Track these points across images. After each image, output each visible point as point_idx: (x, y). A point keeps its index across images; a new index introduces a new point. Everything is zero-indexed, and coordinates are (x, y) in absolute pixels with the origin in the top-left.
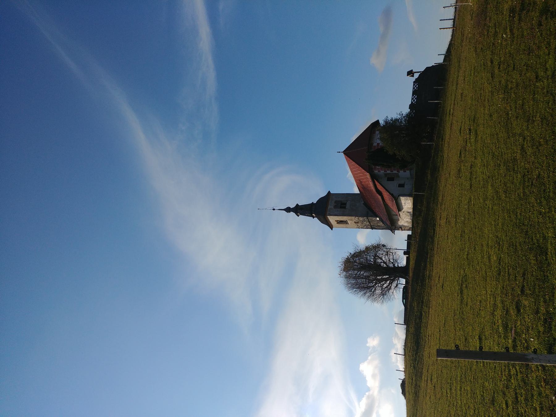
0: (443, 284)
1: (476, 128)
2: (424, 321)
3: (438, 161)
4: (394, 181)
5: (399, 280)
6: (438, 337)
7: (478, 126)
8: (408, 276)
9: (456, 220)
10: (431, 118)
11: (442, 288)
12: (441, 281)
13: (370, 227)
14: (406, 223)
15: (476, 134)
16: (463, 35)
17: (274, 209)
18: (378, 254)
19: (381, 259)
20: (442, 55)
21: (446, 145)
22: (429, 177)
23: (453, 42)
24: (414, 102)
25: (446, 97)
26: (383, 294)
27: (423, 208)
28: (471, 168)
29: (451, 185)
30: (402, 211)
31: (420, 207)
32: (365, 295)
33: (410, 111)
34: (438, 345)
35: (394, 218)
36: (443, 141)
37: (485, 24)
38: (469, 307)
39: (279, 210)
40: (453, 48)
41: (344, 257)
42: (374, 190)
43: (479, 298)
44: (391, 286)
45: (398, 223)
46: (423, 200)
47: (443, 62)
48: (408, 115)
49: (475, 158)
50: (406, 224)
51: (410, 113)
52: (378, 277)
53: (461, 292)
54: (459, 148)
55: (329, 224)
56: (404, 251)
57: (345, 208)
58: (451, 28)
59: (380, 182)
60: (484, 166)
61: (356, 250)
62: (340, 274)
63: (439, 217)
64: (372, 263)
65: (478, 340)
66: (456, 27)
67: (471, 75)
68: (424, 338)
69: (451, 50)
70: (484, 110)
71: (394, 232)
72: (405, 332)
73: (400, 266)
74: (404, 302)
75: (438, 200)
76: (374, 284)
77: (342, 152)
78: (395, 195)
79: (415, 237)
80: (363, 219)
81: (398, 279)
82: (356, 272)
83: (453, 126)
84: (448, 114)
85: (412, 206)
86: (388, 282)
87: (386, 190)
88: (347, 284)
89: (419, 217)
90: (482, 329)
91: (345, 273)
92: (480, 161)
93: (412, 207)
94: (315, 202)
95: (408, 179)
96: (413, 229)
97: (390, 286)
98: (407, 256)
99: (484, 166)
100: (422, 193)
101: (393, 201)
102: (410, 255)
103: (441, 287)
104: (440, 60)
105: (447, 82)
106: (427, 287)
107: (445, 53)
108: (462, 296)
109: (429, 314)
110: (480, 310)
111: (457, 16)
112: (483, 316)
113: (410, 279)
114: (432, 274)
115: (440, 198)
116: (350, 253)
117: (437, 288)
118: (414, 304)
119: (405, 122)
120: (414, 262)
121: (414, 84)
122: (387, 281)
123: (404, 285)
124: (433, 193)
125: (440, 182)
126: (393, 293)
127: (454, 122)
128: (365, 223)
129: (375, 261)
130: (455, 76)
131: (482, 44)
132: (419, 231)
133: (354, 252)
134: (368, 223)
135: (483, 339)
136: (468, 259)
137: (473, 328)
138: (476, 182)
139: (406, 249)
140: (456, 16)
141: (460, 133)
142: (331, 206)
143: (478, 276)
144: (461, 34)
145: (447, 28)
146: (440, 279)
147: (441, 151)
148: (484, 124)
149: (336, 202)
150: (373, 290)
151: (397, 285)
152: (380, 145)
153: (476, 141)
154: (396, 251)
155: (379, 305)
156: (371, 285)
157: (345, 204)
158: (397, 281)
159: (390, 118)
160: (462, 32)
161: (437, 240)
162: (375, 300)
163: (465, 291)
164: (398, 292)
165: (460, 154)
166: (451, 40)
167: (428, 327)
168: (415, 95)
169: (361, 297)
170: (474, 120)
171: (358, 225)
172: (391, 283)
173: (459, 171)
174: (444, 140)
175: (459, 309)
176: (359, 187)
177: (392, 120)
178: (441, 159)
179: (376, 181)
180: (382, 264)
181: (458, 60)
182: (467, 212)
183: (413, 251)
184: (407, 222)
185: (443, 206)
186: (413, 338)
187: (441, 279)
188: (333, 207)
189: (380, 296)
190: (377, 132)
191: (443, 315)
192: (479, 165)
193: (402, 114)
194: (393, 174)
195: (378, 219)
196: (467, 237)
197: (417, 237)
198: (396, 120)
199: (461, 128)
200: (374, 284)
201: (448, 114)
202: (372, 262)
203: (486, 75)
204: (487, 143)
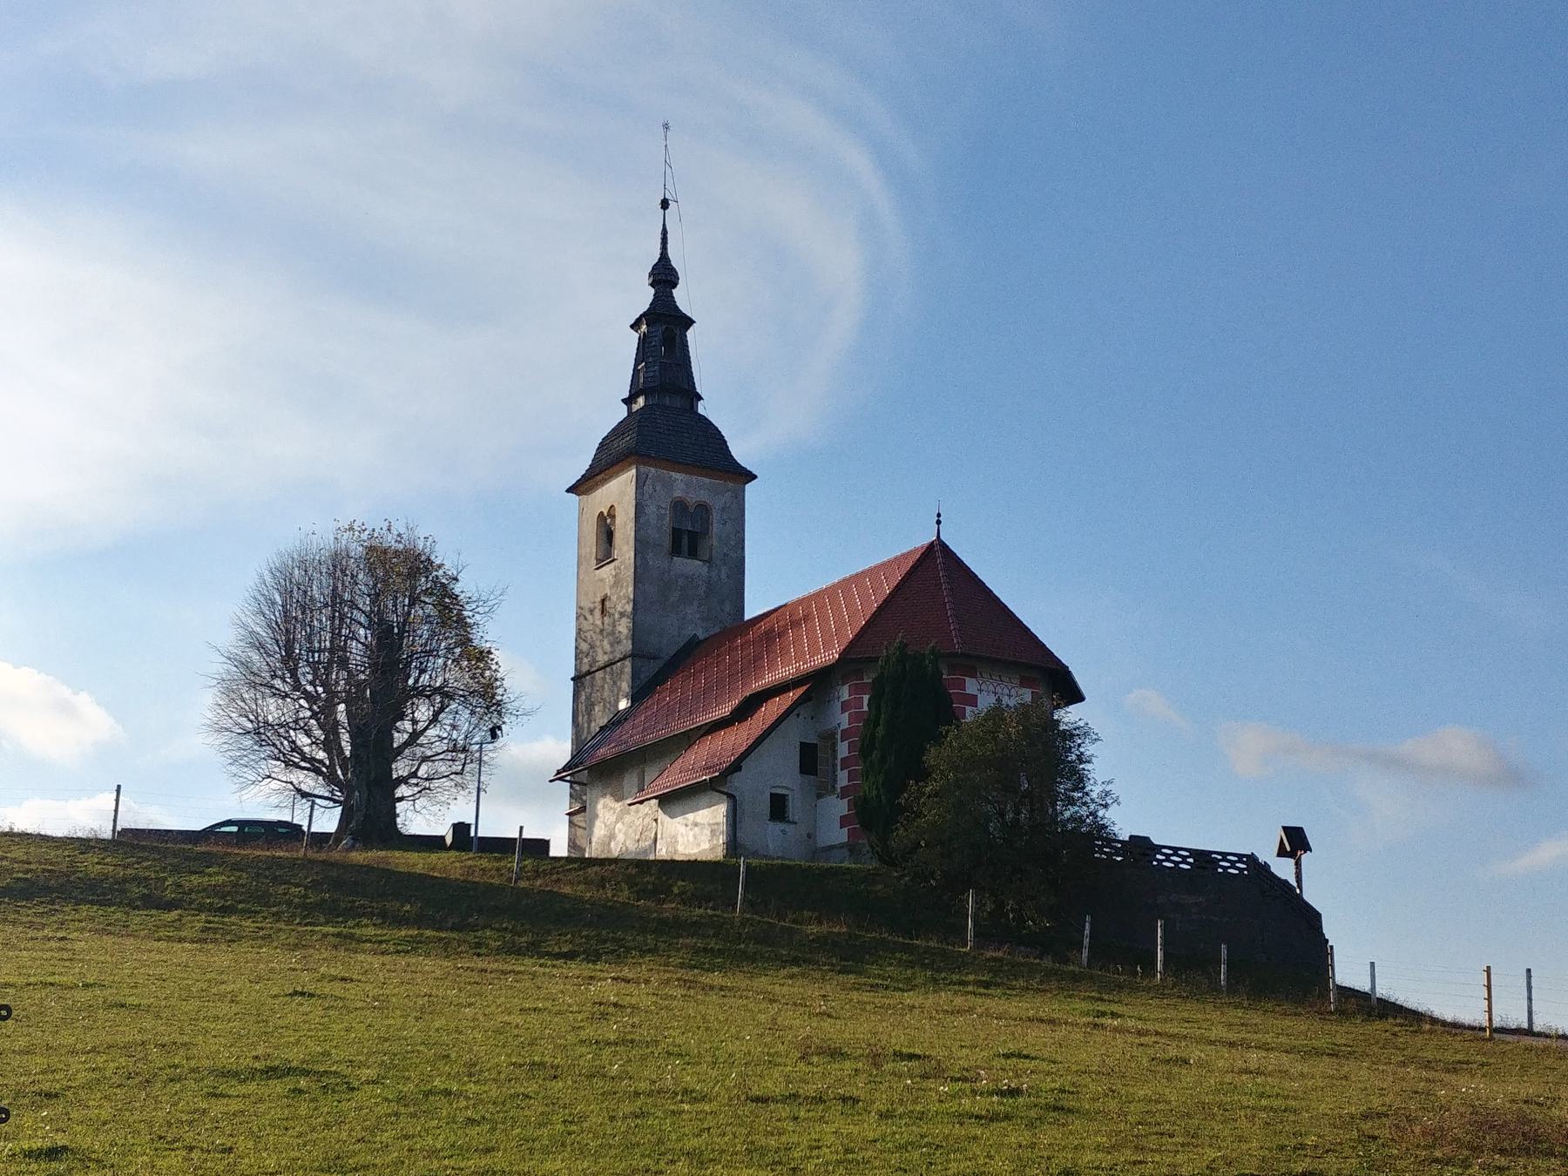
0: (311, 995)
1: (1022, 1118)
2: (137, 918)
3: (891, 965)
4: (802, 772)
5: (331, 804)
6: (57, 979)
7: (1031, 1125)
8: (353, 846)
9: (609, 1044)
10: (1087, 932)
11: (296, 993)
12: (327, 988)
13: (585, 668)
14: (602, 832)
15: (993, 1118)
16: (1453, 1069)
17: (665, 204)
18: (453, 706)
19: (434, 720)
20: (1526, 1014)
21: (958, 1001)
22: (813, 929)
23: (1427, 1027)
24: (1159, 857)
25: (1179, 997)
26: (262, 730)
27: (673, 905)
28: (844, 1099)
29: (774, 1019)
30: (661, 816)
31: (676, 890)
32: (252, 645)
33: (1119, 842)
34: (21, 981)
35: (626, 781)
36: (978, 987)
37: (1477, 1150)
38: (205, 1106)
39: (665, 232)
40: (1396, 1029)
41: (437, 548)
42: (757, 685)
43: (243, 1144)
44: (304, 768)
45: (604, 795)
46: (711, 905)
47: (1337, 985)
48: (1100, 832)
49: (884, 1116)
50: (599, 831)
51: (1110, 840)
52: (342, 707)
53: (274, 1069)
54: (938, 1053)
55: (599, 477)
56: (473, 822)
57: (676, 550)
58: (1490, 1019)
59: (795, 712)
60: (847, 1151)
61: (474, 606)
62: (351, 529)
63: (630, 976)
64: (411, 682)
65: (48, 1144)
66: (1491, 1039)
67: (1262, 1095)
68: (54, 918)
69: (1391, 1020)
70: (1098, 1148)
71: (561, 779)
72: (80, 835)
73: (400, 807)
74: (223, 829)
75: (708, 970)
76: (310, 688)
77: (938, 536)
78: (737, 780)
79: (537, 875)
80: (622, 637)
81: (335, 801)
82: (364, 603)
83: (1043, 1026)
84: (1102, 1007)
85: (680, 859)
86: (321, 755)
87: (759, 741)
88: (303, 565)
89: (629, 889)
90: (98, 1161)
91: (357, 550)
92: (871, 1135)
93: (677, 858)
94: (701, 411)
95: (809, 836)
96: (578, 863)
97: (303, 764)
98: (449, 840)
99: (847, 1151)
100: (744, 900)
101: (707, 768)
102: (453, 853)
103: (299, 989)
104: (1348, 972)
105: (1246, 1003)
106: (300, 929)
107: (1381, 992)
108: (253, 1074)
109: (169, 939)
110: (191, 1149)
111: (1540, 1043)
112: (159, 1163)
113: (336, 856)
114: (364, 951)
115: (716, 978)
116: (456, 579)
117: (294, 970)
118: (217, 874)
119: (1072, 819)
120: (419, 869)
121: (1244, 856)
122: (324, 751)
123: (305, 829)
124: (742, 946)
125: (792, 977)
126: (269, 777)
127: (1062, 1032)
128: (605, 642)
129: (420, 692)
130: (1269, 1038)
131: (1393, 1140)
132: (567, 890)
133: (462, 596)
134: (602, 659)
135: (54, 1165)
136: (427, 1094)
137: (105, 1123)
138: (779, 1120)
139: (479, 835)
140: (1542, 1039)
141: (1007, 1056)
142: (684, 485)
143: (349, 1135)
144: (1459, 1062)
145: (1489, 999)
146: (338, 984)
147: (935, 981)
148: (1033, 1146)
149: (703, 508)
150: (278, 683)
151: (304, 795)
152: (968, 709)
153: (962, 1117)
154: (473, 787)
155: (210, 715)
156: (304, 674)
157: (693, 553)
158: (327, 794)
159: (1088, 753)
160: (1467, 1063)
161: (522, 968)
162: (230, 692)
163: (278, 1087)
164: (274, 800)
165: (911, 1057)
166: (1434, 1021)
167: (108, 940)
168: (1191, 860)
169: (244, 626)
170: (1055, 1109)
171: (591, 611)
172: (315, 767)
173: (836, 1054)
174: (982, 990)
175: (193, 1063)
176: (775, 614)
177: (1081, 762)
178: (898, 981)
179: (800, 691)
180: (407, 726)
181: (1343, 1048)
182: (643, 1086)
183: (470, 863)
184: (612, 837)
185: (679, 992)
186: (49, 871)
187: (337, 988)
188: (678, 494)
189: (252, 717)
190: (1027, 695)
191: (165, 999)
192: (855, 1130)
193: (1106, 806)
194: (834, 765)
195: (623, 704)
196: (531, 1088)
197: (539, 882)
198: (1080, 782)
199: (1026, 1057)
200: (310, 688)
201: (1102, 1007)
202: (417, 681)
203: (1249, 1155)
204: (948, 1161)
